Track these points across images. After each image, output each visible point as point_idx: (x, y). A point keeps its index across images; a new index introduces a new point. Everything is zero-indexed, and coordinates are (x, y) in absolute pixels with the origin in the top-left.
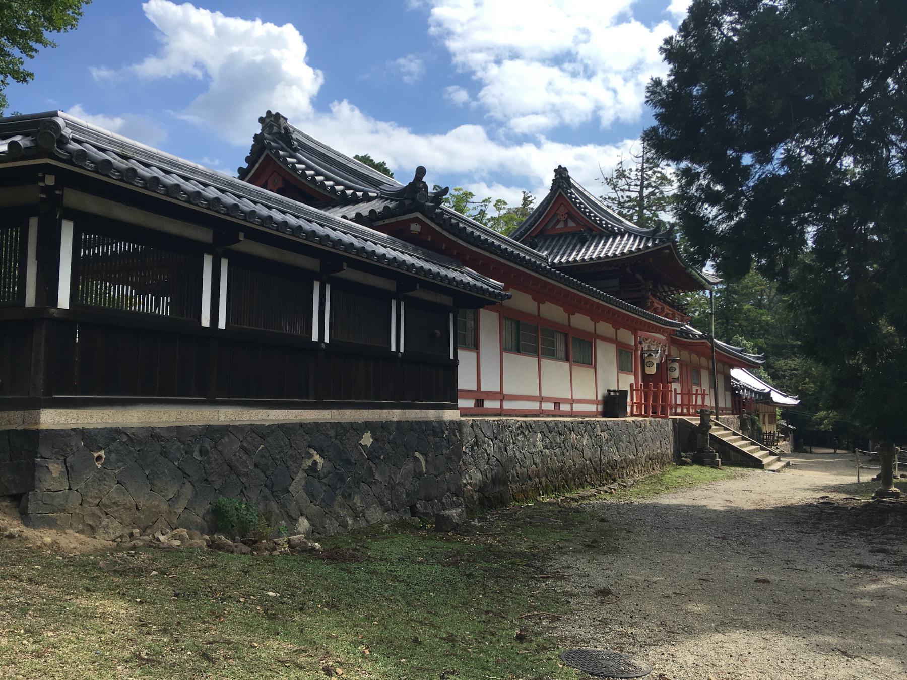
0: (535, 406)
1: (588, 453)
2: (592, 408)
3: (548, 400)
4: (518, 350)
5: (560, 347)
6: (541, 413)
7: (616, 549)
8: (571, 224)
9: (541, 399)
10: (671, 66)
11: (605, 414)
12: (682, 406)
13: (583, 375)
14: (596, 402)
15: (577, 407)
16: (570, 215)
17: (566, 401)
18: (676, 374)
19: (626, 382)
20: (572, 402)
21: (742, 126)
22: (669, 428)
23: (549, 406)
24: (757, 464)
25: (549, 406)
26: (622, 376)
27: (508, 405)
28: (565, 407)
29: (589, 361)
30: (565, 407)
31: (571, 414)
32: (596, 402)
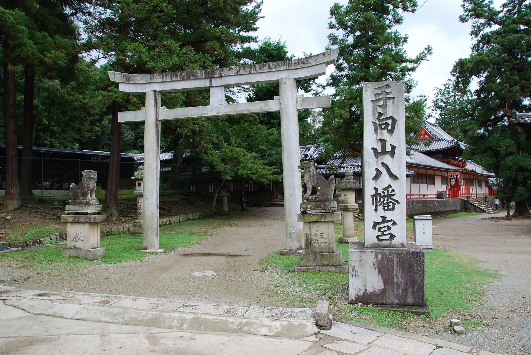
0: (418, 197)
1: (432, 209)
2: (434, 196)
3: (422, 195)
4: (414, 183)
5: (424, 180)
6: (420, 198)
7: (193, 204)
8: (426, 136)
9: (420, 195)
10: (157, 75)
11: (438, 198)
12: (465, 194)
13: (431, 187)
14: (435, 195)
15: (429, 196)
16: (426, 133)
17: (426, 195)
18: (462, 184)
19: (444, 188)
20: (428, 195)
21: (216, 69)
22: (458, 201)
23: (422, 196)
24: (373, 205)
25: (422, 196)
26: (412, 185)
27: (412, 197)
28: (426, 197)
29: (433, 183)
30: (426, 197)
31: (428, 198)
32: (435, 195)
